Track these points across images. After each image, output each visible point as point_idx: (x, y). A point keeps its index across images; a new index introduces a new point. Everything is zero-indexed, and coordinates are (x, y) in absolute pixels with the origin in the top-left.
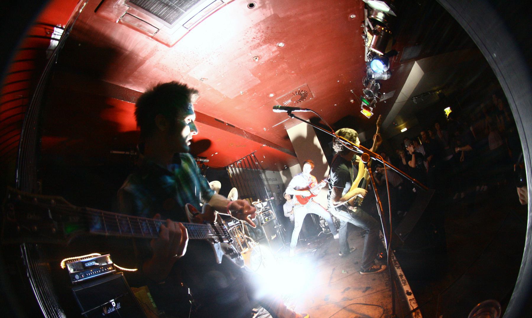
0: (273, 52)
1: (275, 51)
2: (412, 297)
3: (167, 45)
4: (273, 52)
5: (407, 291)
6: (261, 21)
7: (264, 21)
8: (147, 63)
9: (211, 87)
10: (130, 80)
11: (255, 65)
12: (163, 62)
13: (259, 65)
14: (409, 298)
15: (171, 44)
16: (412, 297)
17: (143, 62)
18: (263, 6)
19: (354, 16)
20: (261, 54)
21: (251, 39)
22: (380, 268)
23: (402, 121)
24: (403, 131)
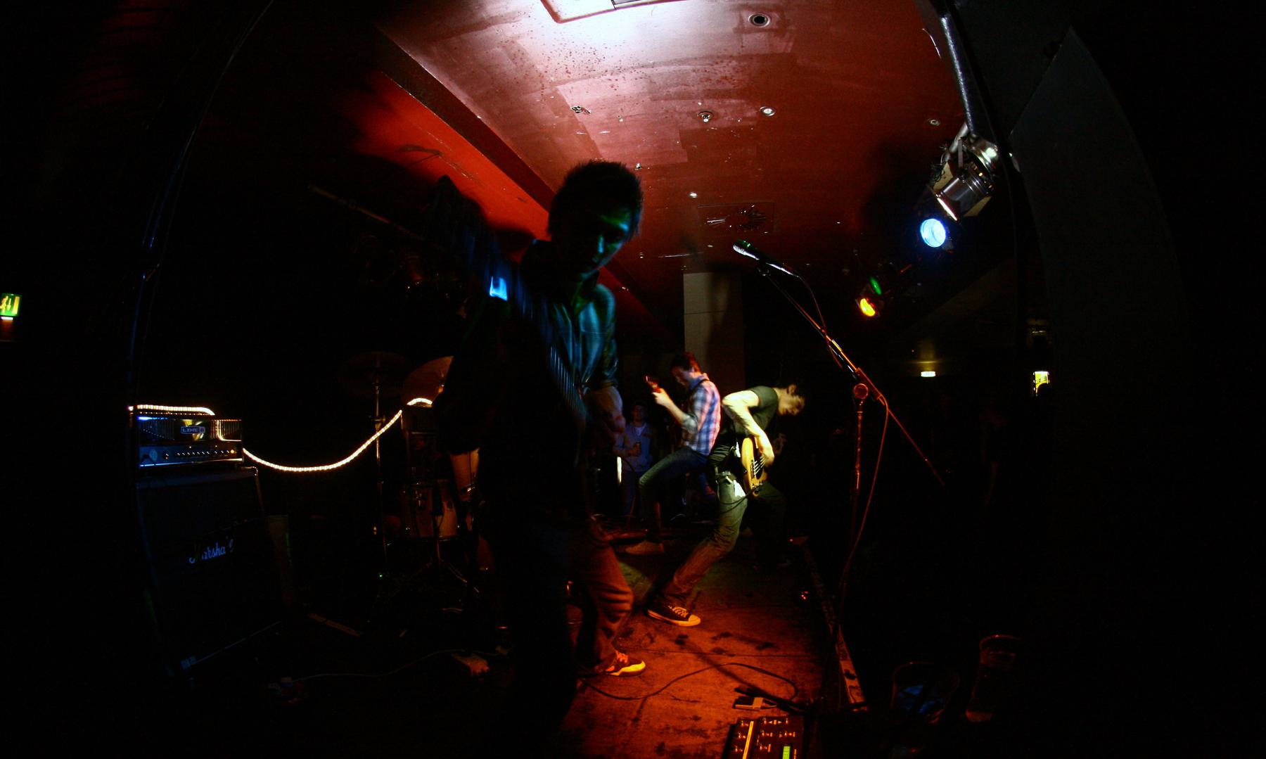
0: (744, 119)
1: (751, 119)
2: (855, 683)
3: (555, 16)
4: (744, 119)
5: (847, 672)
6: (758, 55)
7: (764, 58)
8: (493, 31)
9: (584, 130)
10: (434, 50)
11: (697, 126)
12: (525, 43)
13: (703, 130)
14: (849, 682)
15: (563, 17)
16: (855, 683)
17: (484, 24)
18: (779, 31)
19: (937, 123)
20: (722, 111)
21: (718, 76)
22: (686, 619)
23: (931, 356)
24: (924, 374)
